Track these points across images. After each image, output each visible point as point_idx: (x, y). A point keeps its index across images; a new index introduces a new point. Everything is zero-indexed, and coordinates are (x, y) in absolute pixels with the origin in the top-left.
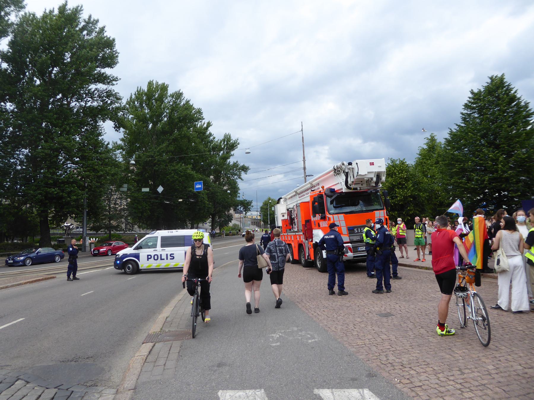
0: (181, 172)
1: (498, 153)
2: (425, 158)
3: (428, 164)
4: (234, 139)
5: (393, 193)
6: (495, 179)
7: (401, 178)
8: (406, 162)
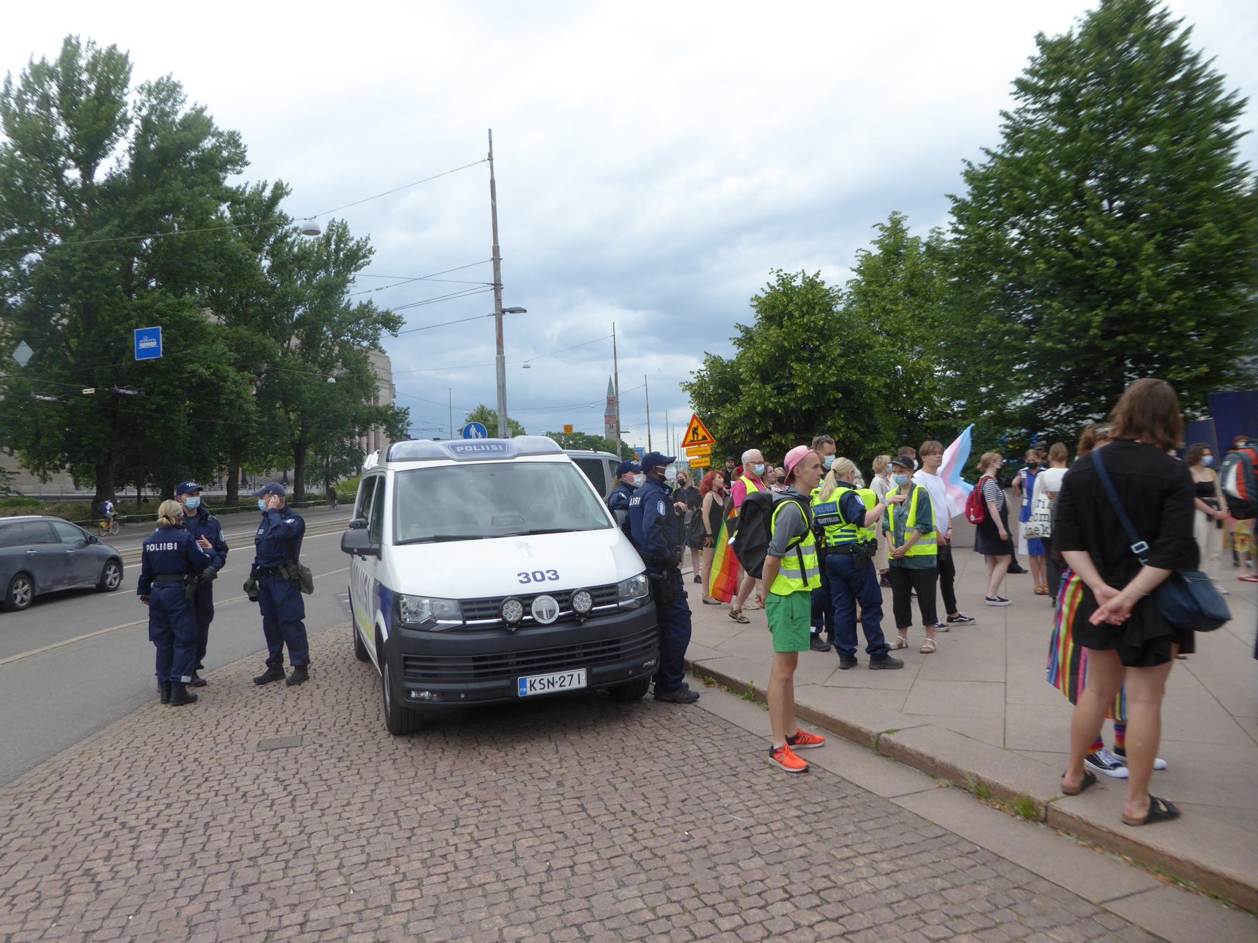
0: (162, 315)
1: (1136, 229)
2: (877, 282)
3: (884, 298)
4: (357, 238)
5: (782, 377)
6: (1125, 319)
7: (808, 329)
8: (823, 283)
